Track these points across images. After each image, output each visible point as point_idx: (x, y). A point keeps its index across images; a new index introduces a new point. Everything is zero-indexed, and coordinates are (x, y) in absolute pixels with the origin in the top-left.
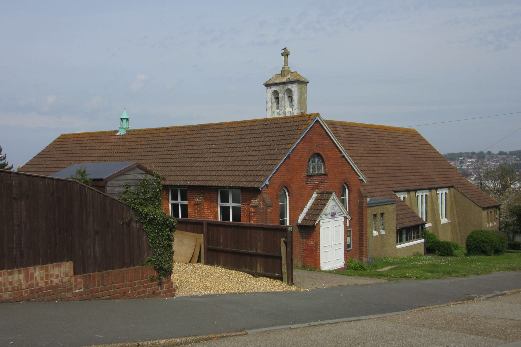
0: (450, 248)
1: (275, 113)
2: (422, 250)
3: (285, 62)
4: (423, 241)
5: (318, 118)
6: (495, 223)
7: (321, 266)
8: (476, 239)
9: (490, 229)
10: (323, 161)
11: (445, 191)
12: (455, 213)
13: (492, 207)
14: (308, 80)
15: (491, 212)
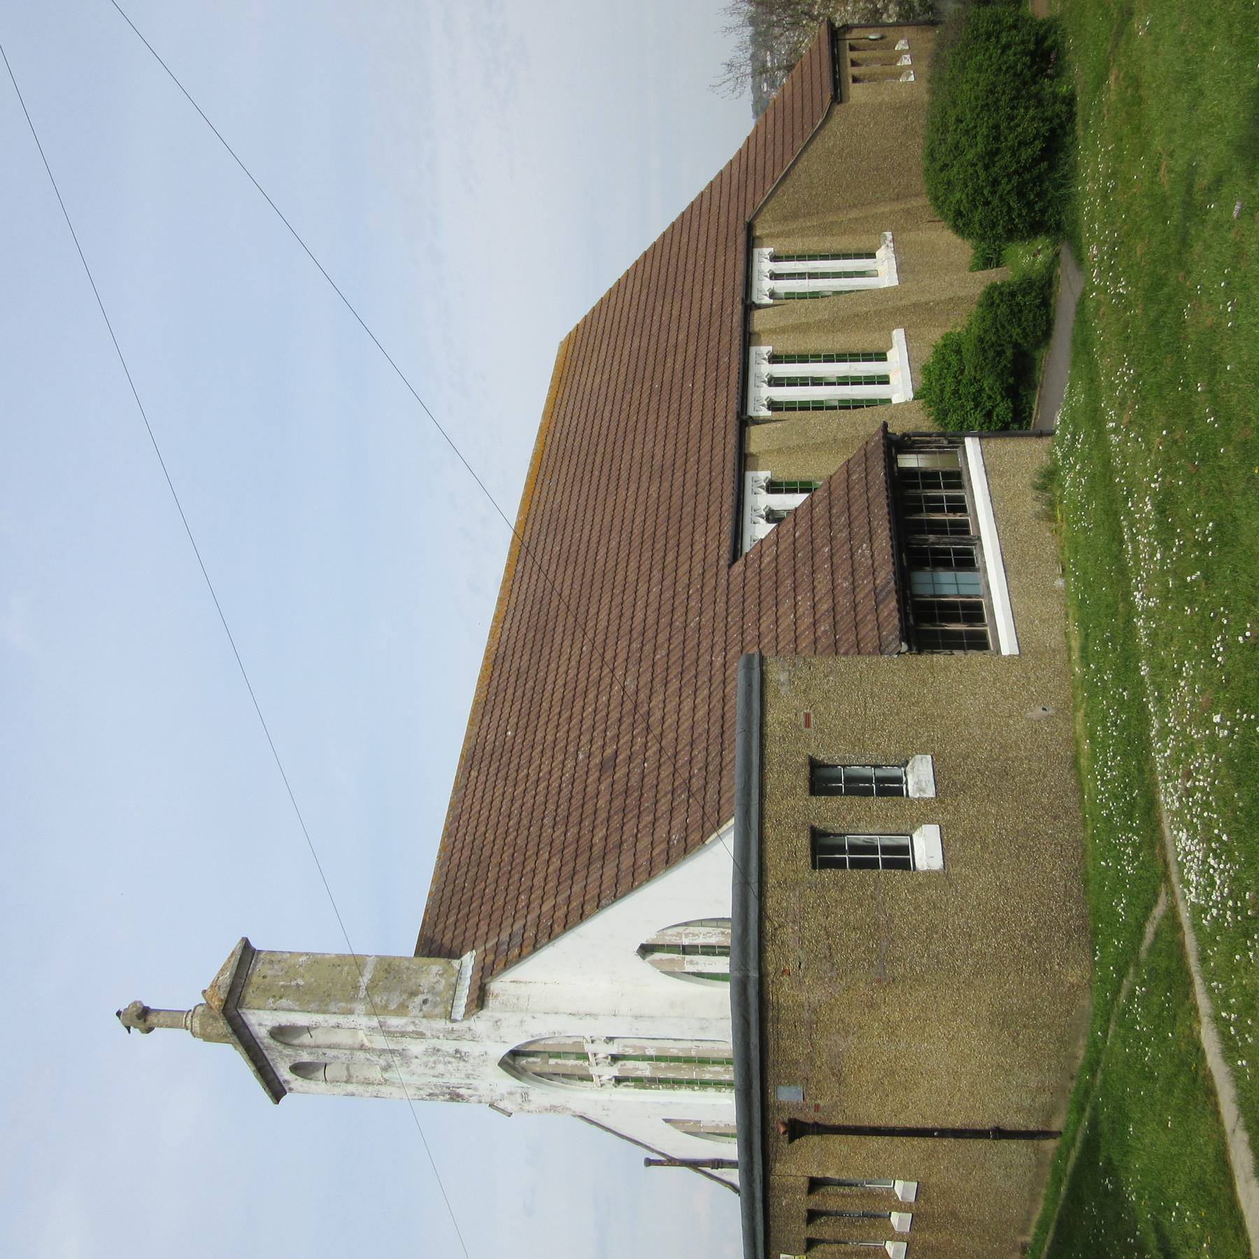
0: (1013, 295)
1: (386, 1075)
2: (1027, 454)
3: (174, 1019)
4: (972, 446)
6: (901, 45)
8: (978, 191)
9: (924, 66)
11: (763, 264)
12: (854, 214)
13: (835, 60)
14: (233, 944)
15: (854, 64)
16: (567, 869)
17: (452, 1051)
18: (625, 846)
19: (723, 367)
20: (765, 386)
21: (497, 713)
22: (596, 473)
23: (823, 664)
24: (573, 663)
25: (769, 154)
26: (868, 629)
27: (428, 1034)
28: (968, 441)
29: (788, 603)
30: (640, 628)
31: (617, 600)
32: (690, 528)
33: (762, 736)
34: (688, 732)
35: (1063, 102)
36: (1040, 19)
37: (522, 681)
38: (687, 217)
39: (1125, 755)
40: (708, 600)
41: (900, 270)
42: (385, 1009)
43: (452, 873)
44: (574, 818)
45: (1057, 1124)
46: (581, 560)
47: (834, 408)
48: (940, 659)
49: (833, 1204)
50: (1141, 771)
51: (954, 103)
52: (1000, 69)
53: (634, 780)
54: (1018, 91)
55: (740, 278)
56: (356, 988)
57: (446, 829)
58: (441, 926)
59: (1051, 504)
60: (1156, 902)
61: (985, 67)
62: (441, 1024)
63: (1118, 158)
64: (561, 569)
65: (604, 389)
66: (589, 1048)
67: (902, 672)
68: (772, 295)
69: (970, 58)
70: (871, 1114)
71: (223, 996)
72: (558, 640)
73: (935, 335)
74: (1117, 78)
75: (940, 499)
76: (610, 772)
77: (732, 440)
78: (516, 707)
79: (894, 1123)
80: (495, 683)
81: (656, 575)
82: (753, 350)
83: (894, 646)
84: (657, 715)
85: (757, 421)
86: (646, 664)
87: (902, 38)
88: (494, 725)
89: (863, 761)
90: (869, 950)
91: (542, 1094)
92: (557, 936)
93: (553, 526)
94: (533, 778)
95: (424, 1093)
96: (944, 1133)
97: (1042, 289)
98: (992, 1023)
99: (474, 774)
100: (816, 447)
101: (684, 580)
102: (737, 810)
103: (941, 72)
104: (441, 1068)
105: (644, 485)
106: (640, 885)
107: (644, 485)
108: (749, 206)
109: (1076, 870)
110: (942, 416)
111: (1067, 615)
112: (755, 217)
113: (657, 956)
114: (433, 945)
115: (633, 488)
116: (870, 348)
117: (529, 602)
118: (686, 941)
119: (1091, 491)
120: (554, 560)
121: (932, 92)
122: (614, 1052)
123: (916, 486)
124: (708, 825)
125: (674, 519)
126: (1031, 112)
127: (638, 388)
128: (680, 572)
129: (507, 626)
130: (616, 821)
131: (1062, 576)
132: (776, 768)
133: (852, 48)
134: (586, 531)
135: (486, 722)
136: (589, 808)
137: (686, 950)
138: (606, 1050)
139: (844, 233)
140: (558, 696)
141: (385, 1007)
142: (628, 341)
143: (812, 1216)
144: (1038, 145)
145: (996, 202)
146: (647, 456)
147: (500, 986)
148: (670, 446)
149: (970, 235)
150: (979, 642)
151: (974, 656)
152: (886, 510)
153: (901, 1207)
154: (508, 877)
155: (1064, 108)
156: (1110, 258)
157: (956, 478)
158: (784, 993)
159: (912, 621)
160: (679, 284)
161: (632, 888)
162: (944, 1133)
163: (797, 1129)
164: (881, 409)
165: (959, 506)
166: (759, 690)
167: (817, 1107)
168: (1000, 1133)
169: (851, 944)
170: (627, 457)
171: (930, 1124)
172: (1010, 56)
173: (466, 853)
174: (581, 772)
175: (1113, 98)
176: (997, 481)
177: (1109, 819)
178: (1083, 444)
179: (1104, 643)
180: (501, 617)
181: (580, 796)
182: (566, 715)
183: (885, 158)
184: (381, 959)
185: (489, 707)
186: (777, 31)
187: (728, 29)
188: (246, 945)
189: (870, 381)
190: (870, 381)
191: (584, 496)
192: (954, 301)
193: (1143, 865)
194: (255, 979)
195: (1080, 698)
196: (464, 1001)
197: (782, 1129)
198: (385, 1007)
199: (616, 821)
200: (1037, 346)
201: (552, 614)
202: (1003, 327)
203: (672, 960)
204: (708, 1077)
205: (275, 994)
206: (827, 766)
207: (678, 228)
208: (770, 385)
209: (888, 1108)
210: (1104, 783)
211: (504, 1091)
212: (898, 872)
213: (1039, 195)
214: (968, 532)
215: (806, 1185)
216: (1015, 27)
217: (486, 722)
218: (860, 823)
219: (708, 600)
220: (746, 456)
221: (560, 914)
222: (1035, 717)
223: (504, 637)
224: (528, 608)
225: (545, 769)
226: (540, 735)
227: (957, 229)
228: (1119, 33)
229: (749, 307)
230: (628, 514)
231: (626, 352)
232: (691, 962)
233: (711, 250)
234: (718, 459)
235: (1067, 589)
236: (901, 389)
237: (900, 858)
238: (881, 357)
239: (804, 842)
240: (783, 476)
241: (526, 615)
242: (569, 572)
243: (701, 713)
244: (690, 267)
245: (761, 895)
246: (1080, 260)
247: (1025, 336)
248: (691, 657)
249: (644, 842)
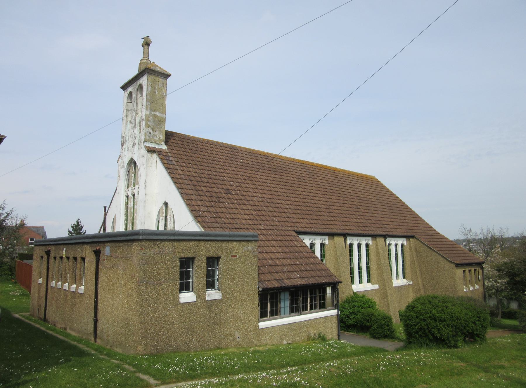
0: (388, 326)
2: (332, 331)
3: (146, 54)
6: (477, 286)
8: (422, 314)
9: (469, 295)
11: (400, 242)
12: (418, 271)
13: (471, 264)
14: (169, 71)
15: (470, 271)
16: (193, 178)
18: (199, 197)
19: (364, 228)
20: (358, 242)
22: (329, 188)
23: (255, 261)
25: (438, 243)
26: (268, 277)
27: (140, 135)
28: (336, 311)
29: (280, 250)
30: (275, 202)
31: (285, 194)
32: (309, 218)
34: (237, 217)
35: (455, 344)
36: (486, 335)
37: (259, 164)
38: (417, 216)
39: (214, 367)
40: (283, 224)
41: (399, 287)
42: (147, 120)
43: (195, 142)
44: (210, 181)
45: (98, 340)
46: (299, 183)
47: (351, 265)
48: (257, 301)
49: (78, 265)
50: (206, 374)
51: (454, 305)
52: (466, 321)
54: (459, 328)
55: (395, 234)
56: (155, 111)
57: (210, 141)
58: (177, 139)
59: (313, 339)
60: (155, 379)
61: (468, 316)
62: (143, 139)
63: (432, 366)
64: (296, 177)
65: (358, 190)
66: (137, 186)
67: (252, 288)
68: (389, 245)
69: (470, 311)
70: (102, 278)
71: (151, 68)
72: (272, 176)
73: (376, 299)
74: (462, 366)
75: (315, 301)
76: (225, 192)
77: (339, 231)
78: (250, 163)
79: (99, 286)
80: (259, 156)
81: (293, 207)
82: (370, 238)
83: (261, 285)
84: (244, 207)
85: (345, 240)
86: (262, 204)
87: (479, 287)
88: (244, 156)
89: (220, 275)
90: (150, 277)
91: (123, 172)
92: (170, 175)
93: (311, 174)
94: (225, 168)
95: (124, 135)
96: (96, 303)
97: (391, 335)
98: (126, 319)
99: (228, 149)
100: (336, 260)
101: (291, 216)
102: (207, 232)
103: (467, 301)
104: (131, 139)
105: (324, 203)
106: (185, 202)
107: (324, 203)
108: (420, 236)
109: (179, 349)
110: (348, 301)
111: (272, 345)
112: (416, 238)
113: (164, 208)
114: (169, 136)
115: (324, 199)
116: (372, 277)
117: (286, 167)
118: (168, 217)
119: (314, 354)
120: (300, 175)
121: (458, 298)
122: (135, 195)
123: (320, 293)
124: (204, 223)
125: (312, 213)
126: (450, 333)
127: (358, 201)
128: (293, 215)
131: (287, 343)
132: (217, 245)
133: (475, 270)
134: (309, 185)
135: (246, 153)
136: (213, 185)
137: (166, 217)
138: (136, 192)
139: (411, 268)
141: (148, 120)
142: (374, 198)
143: (75, 258)
144: (439, 335)
145: (418, 320)
146: (334, 204)
147: (155, 156)
148: (337, 211)
149: (406, 311)
150: (263, 315)
151: (258, 313)
152: (311, 283)
153: (77, 288)
154: (189, 159)
155: (452, 345)
156: (394, 363)
157: (323, 307)
158: (136, 248)
159: (270, 292)
160: (393, 214)
161: (184, 199)
162: (96, 303)
163: (97, 253)
164: (350, 281)
165: (313, 307)
166: (246, 240)
167: (104, 260)
168: (96, 321)
169: (152, 271)
170: (334, 197)
171: (99, 298)
172: (471, 325)
173: (201, 147)
174: (226, 183)
175: (454, 365)
176: (322, 321)
177: (193, 361)
178: (333, 351)
179: (258, 360)
181: (217, 182)
183: (437, 282)
184: (165, 119)
185: (251, 154)
186: (482, 246)
187: (482, 230)
188: (169, 76)
189: (360, 277)
190: (360, 277)
191: (321, 184)
192: (388, 305)
193: (170, 374)
194: (157, 79)
195: (241, 350)
196: (150, 146)
197: (97, 248)
198: (148, 120)
200: (371, 334)
202: (377, 322)
203: (163, 213)
204: (128, 225)
205: (152, 85)
206: (218, 263)
207: (413, 213)
208: (358, 244)
209: (103, 284)
210: (206, 359)
211: (124, 160)
212: (179, 287)
213: (421, 335)
214: (303, 310)
215: (83, 257)
216: (482, 326)
217: (246, 153)
218: (198, 274)
219: (283, 224)
220: (333, 236)
221: (177, 176)
222: (236, 334)
226: (240, 170)
227: (408, 307)
228: (479, 367)
229: (385, 237)
230: (315, 198)
231: (370, 197)
232: (162, 219)
233: (405, 224)
234: (332, 227)
235: (283, 345)
236: (357, 287)
237: (184, 287)
238: (369, 281)
239: (190, 255)
240: (326, 248)
241: (281, 166)
242: (296, 179)
243: (243, 221)
244: (399, 217)
245: (170, 240)
246: (397, 350)
247: (374, 330)
248: (263, 218)
249: (199, 203)
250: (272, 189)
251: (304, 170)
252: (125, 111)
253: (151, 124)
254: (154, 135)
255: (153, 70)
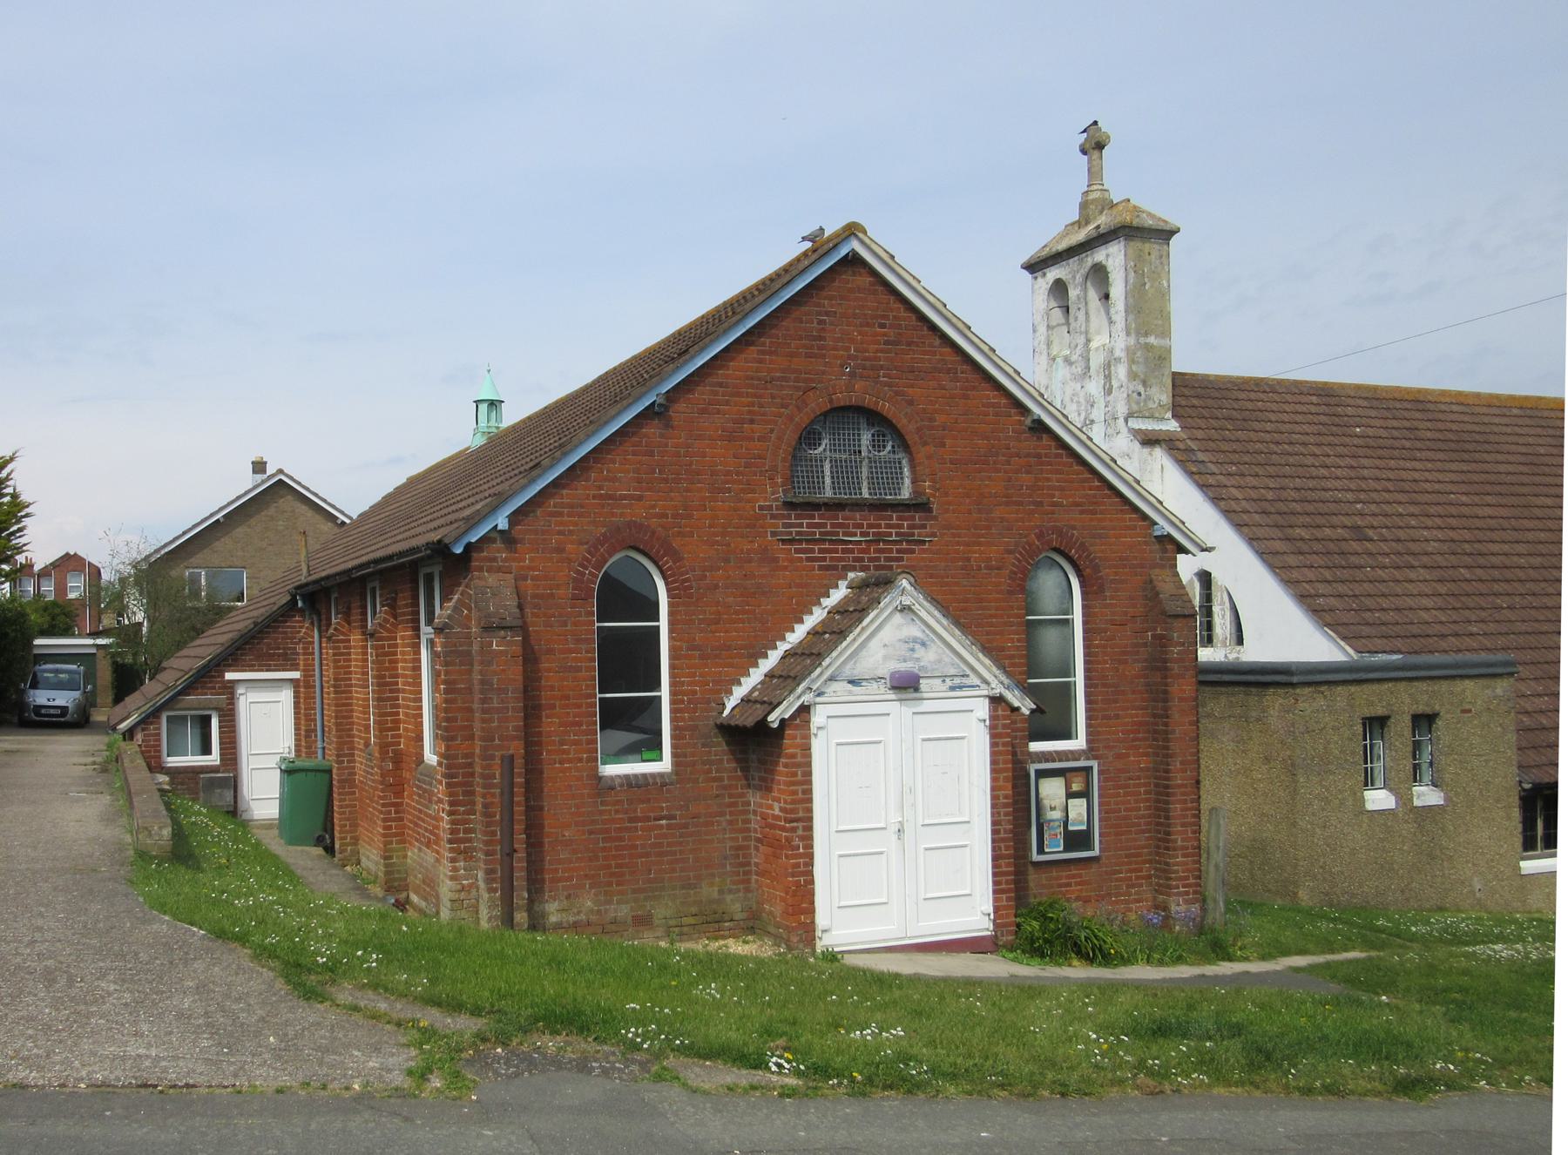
1: (1059, 360)
3: (1094, 174)
5: (855, 245)
7: (821, 920)
10: (903, 444)
14: (1173, 220)
17: (1092, 417)
21: (1373, 413)
24: (1437, 486)
27: (1110, 398)
31: (1505, 524)
33: (1453, 677)
42: (1132, 361)
46: (1537, 479)
48: (1516, 813)
53: (1354, 560)
56: (1146, 334)
57: (1262, 379)
62: (1122, 409)
71: (1135, 223)
72: (1454, 466)
78: (1383, 433)
80: (1398, 405)
81: (1537, 561)
84: (1412, 575)
94: (1328, 461)
99: (1314, 399)
129: (1454, 408)
130: (1317, 547)
135: (1360, 402)
136: (1320, 520)
140: (1404, 475)
147: (1159, 453)
151: (1518, 841)
158: (1275, 702)
166: (1488, 673)
173: (1249, 405)
174: (1346, 508)
180: (1462, 400)
182: (1390, 485)
185: (1375, 403)
199: (1317, 547)
201: (1477, 456)
217: (1360, 402)
223: (1443, 407)
224: (1477, 428)
225: (1339, 472)
226: (1365, 462)
237: (1368, 781)
239: (1380, 711)
243: (1425, 615)
248: (1470, 602)
249: (1310, 575)
250: (1465, 510)
251: (1539, 431)
252: (1042, 329)
253: (1139, 369)
254: (1148, 398)
255: (1138, 229)
